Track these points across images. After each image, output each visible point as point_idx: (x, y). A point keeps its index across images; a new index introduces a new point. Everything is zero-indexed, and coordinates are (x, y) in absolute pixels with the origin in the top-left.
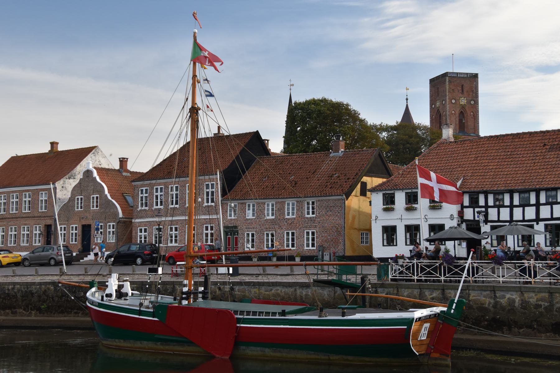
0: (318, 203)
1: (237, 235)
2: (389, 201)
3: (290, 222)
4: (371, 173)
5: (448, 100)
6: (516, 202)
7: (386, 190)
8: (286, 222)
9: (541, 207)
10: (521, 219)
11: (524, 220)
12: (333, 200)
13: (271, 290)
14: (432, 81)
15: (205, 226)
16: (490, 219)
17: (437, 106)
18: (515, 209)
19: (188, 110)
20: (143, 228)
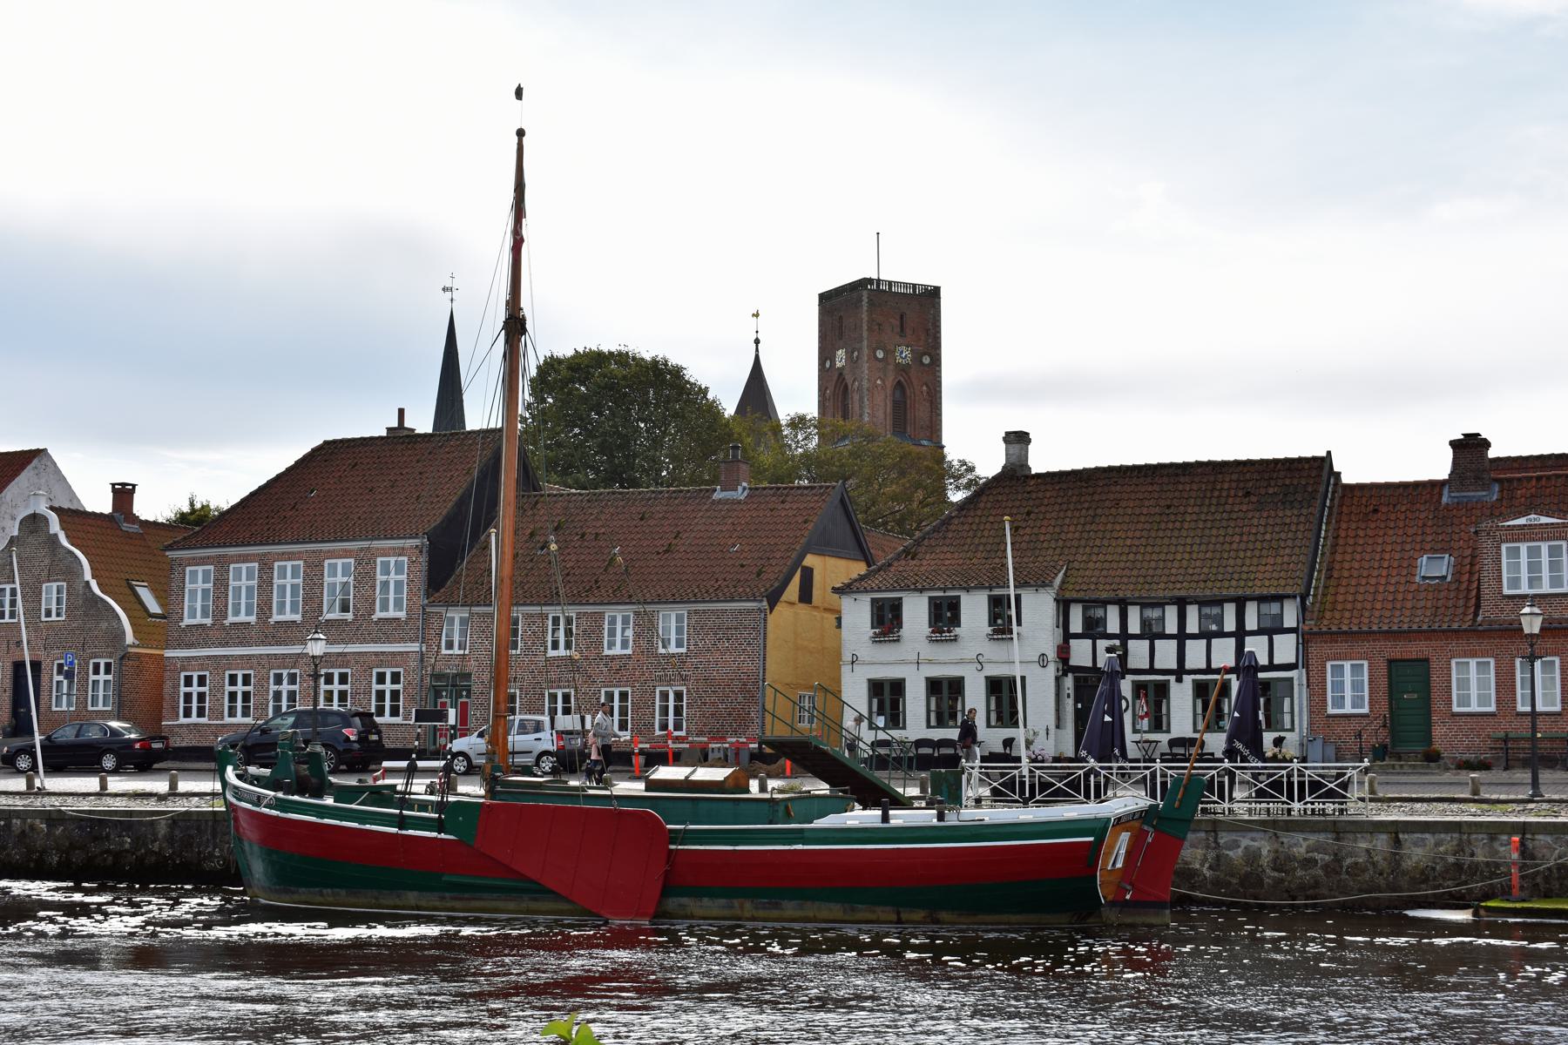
0: (695, 618)
1: (468, 696)
2: (887, 621)
3: (615, 665)
4: (824, 546)
5: (866, 351)
6: (1134, 627)
7: (879, 590)
9: (1247, 639)
10: (1203, 666)
11: (1209, 670)
12: (733, 611)
14: (825, 298)
15: (375, 671)
17: (838, 365)
20: (240, 674)
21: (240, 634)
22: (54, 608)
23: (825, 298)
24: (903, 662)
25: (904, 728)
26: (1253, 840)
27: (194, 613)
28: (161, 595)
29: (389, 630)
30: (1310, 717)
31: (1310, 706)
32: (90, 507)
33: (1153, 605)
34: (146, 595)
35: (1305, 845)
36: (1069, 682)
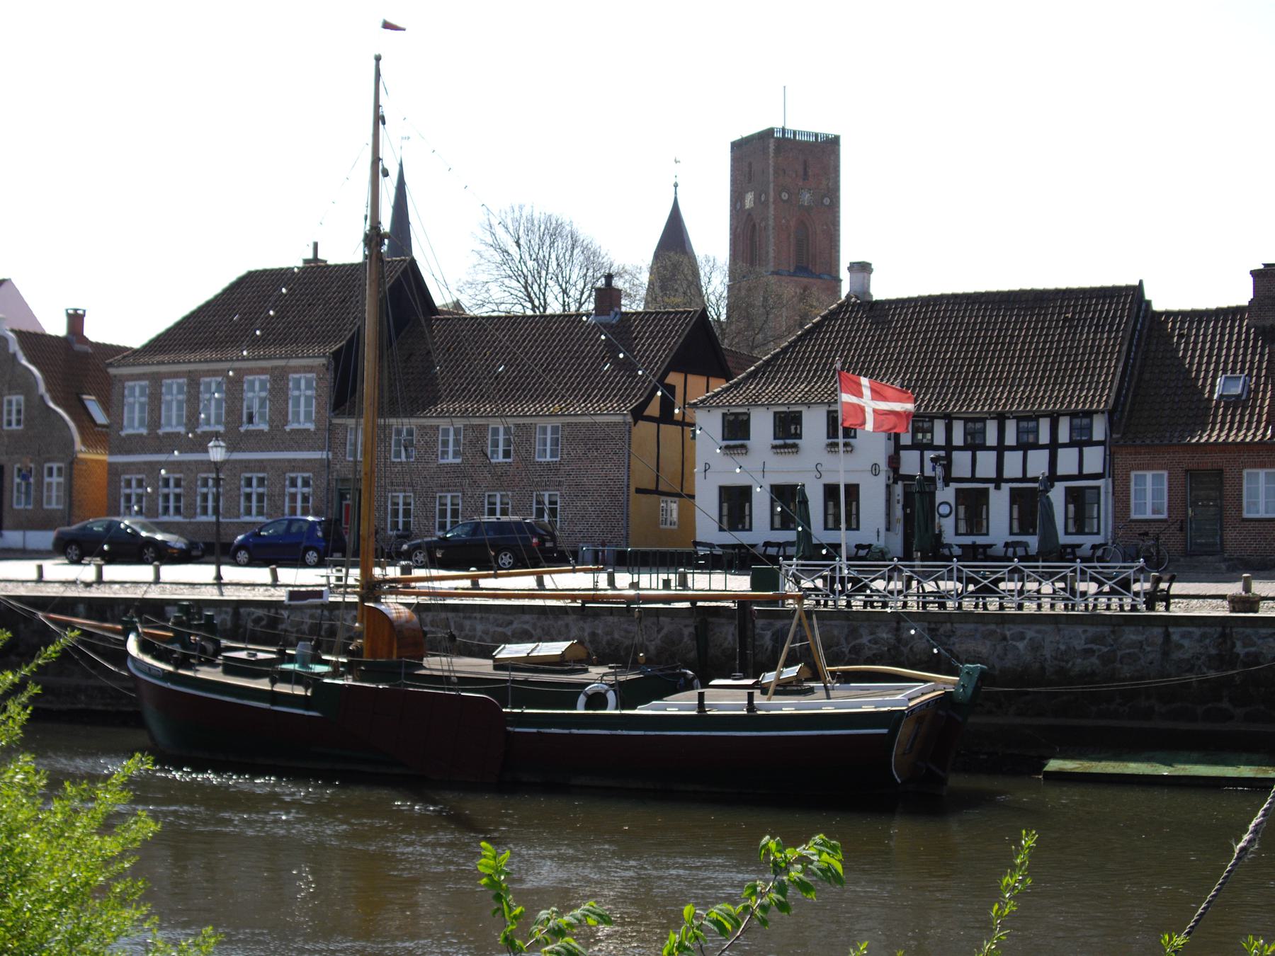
2: (736, 429)
5: (772, 194)
6: (958, 439)
8: (489, 472)
10: (1020, 475)
11: (1024, 479)
13: (511, 623)
14: (738, 147)
16: (955, 474)
18: (1007, 454)
22: (14, 417)
23: (738, 147)
25: (987, 534)
27: (134, 424)
28: (106, 405)
29: (300, 440)
31: (1115, 512)
33: (974, 420)
35: (1083, 637)
36: (899, 489)
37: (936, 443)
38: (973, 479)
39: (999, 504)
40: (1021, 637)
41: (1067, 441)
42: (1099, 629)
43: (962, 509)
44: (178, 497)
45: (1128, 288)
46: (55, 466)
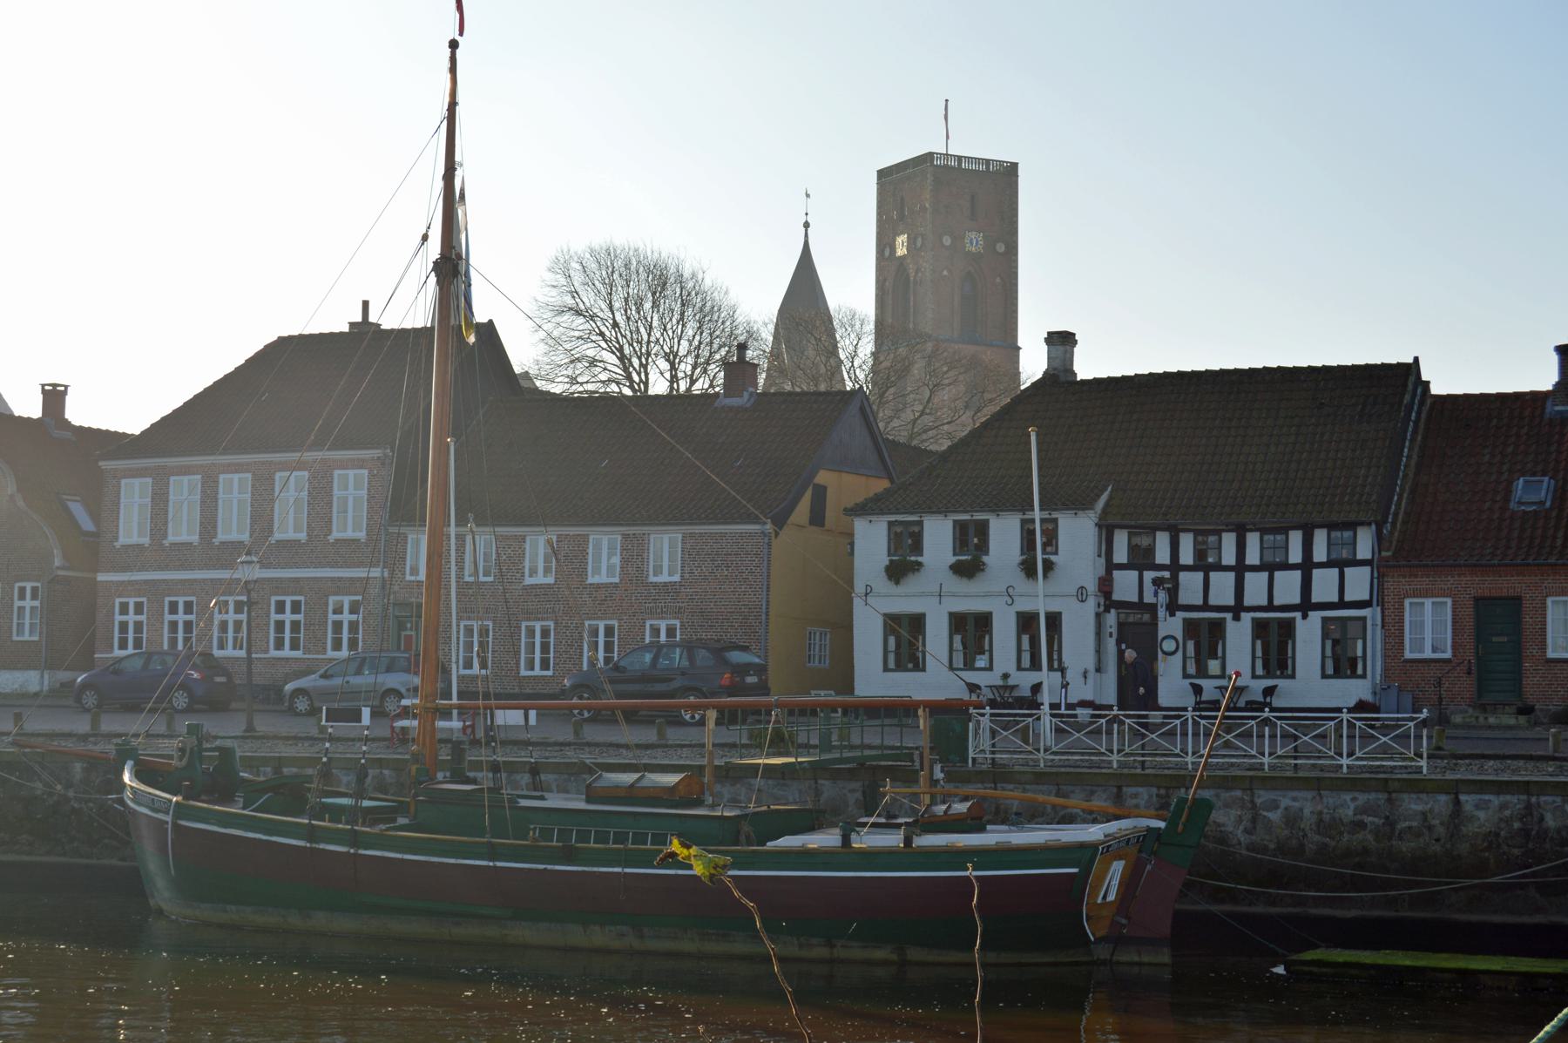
6: (1187, 557)
10: (1264, 602)
11: (1270, 607)
18: (1248, 575)
19: (431, 266)
21: (180, 556)
24: (922, 595)
26: (1294, 799)
27: (131, 529)
28: (95, 517)
29: (347, 552)
30: (1385, 663)
32: (19, 411)
34: (77, 510)
35: (1352, 806)
36: (1111, 619)
37: (1224, 562)
38: (1206, 607)
39: (1239, 638)
40: (1274, 806)
41: (1324, 559)
42: (1372, 796)
43: (1191, 645)
44: (188, 625)
45: (1400, 366)
46: (29, 586)
